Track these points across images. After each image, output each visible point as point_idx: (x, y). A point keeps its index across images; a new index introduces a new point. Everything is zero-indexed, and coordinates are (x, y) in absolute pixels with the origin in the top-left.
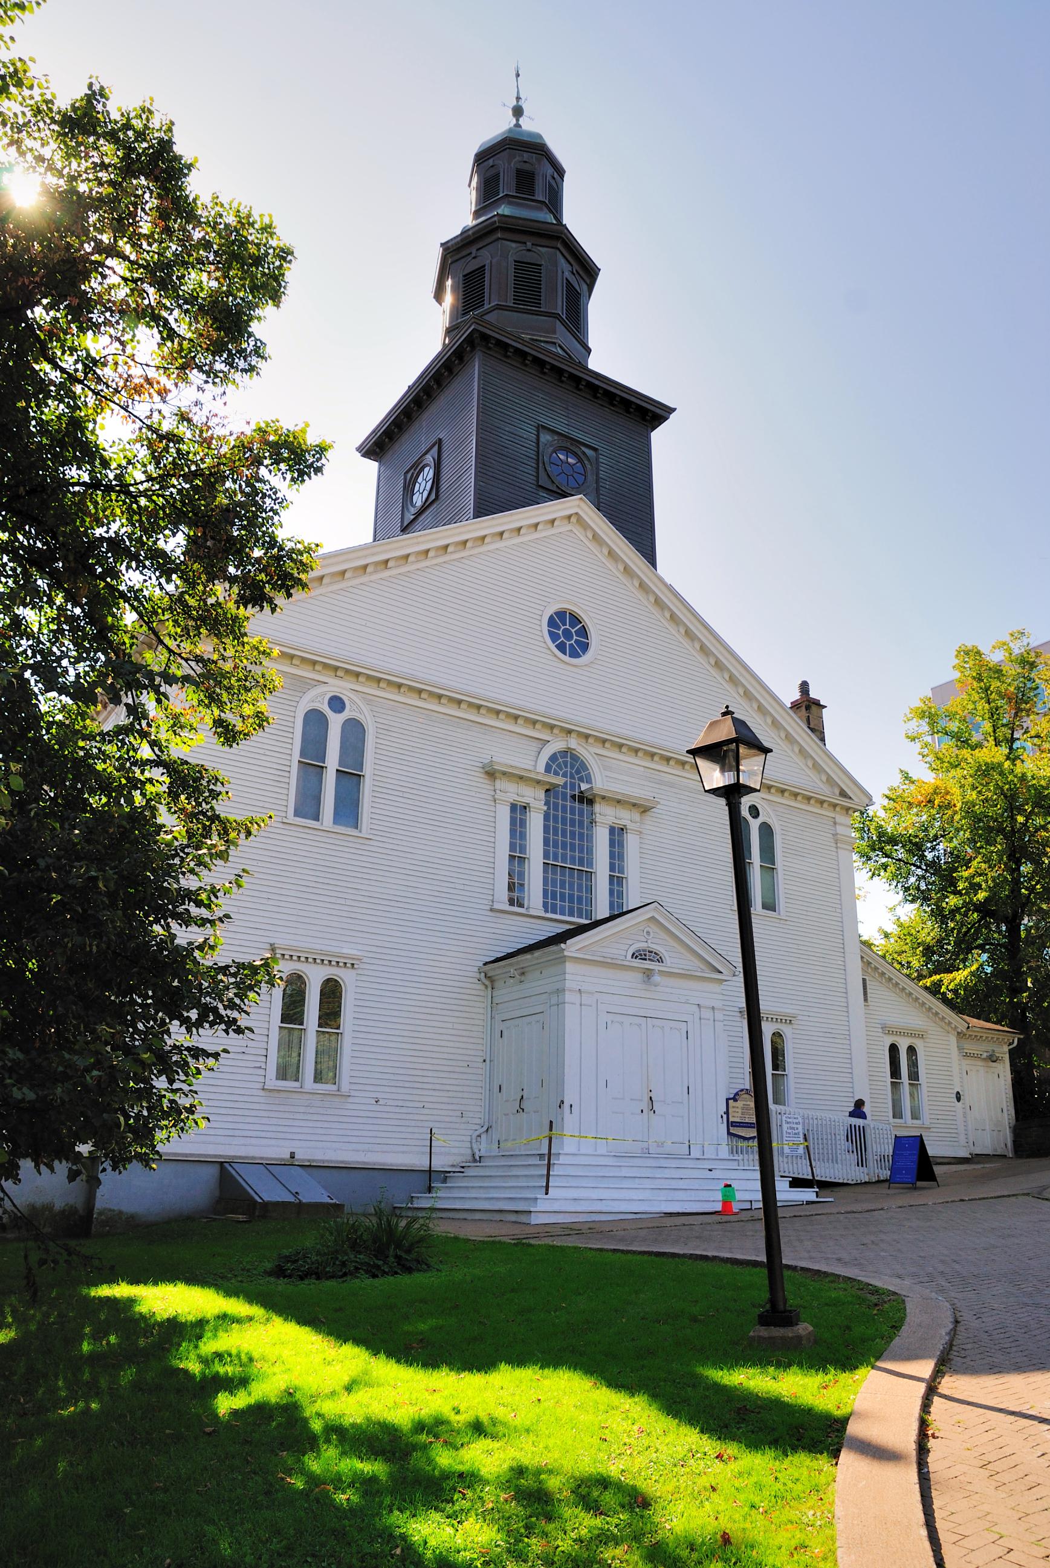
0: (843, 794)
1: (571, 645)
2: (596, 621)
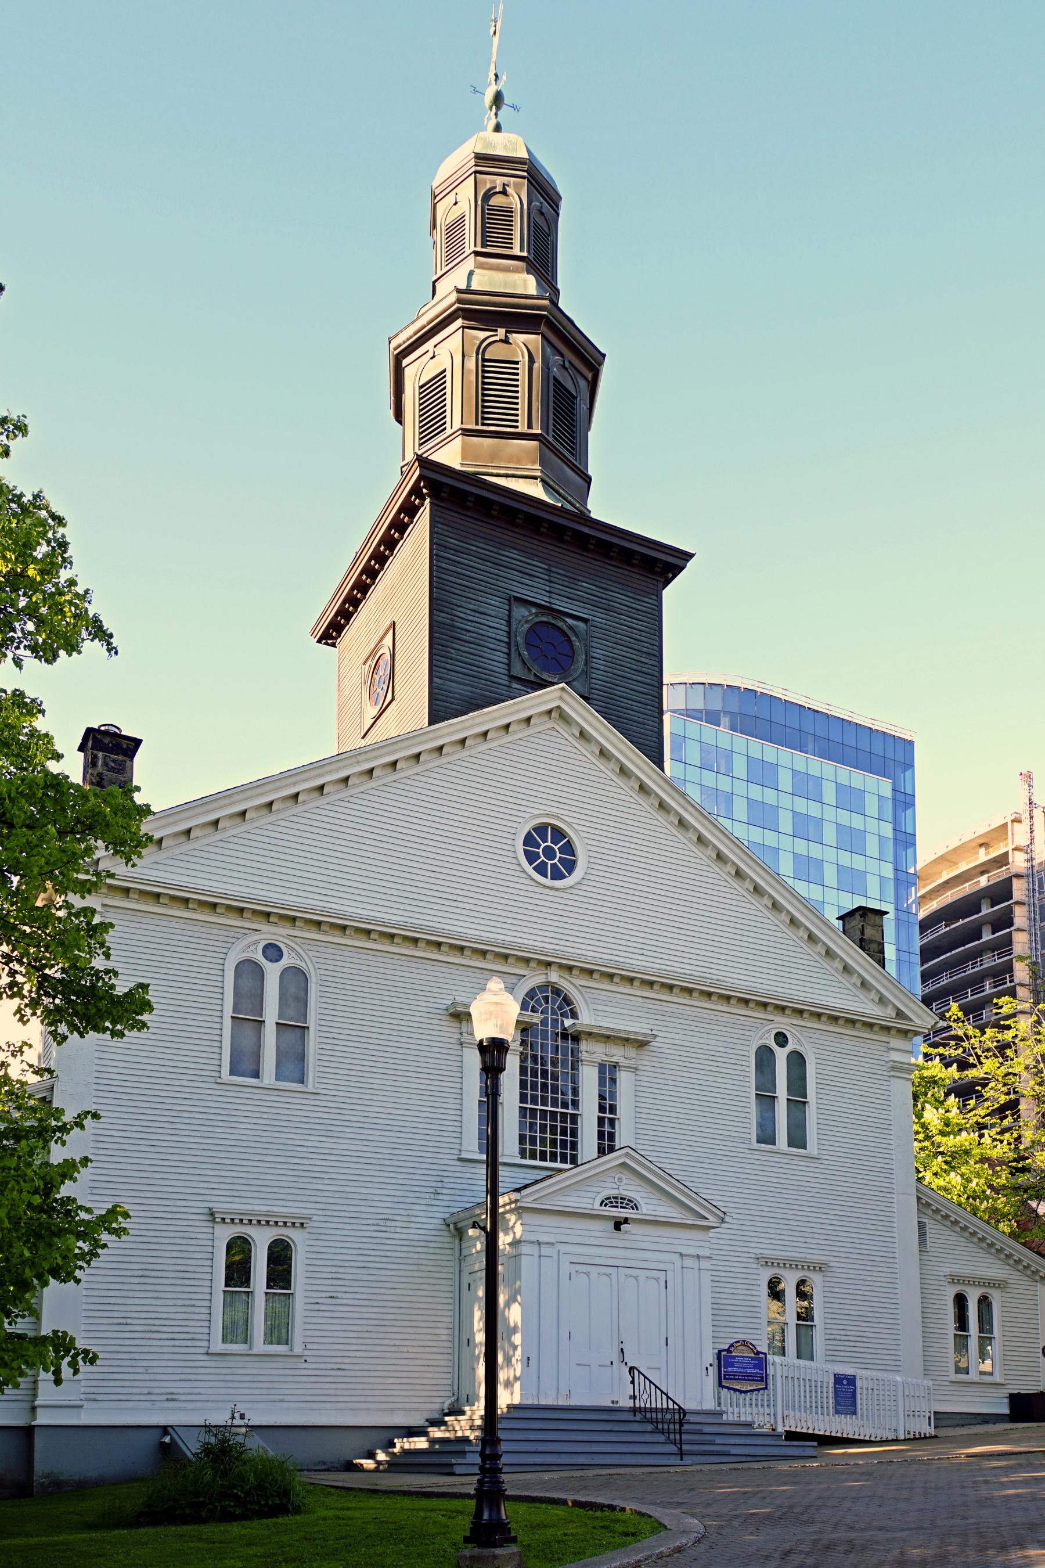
0: (900, 1014)
1: (553, 866)
2: (583, 834)
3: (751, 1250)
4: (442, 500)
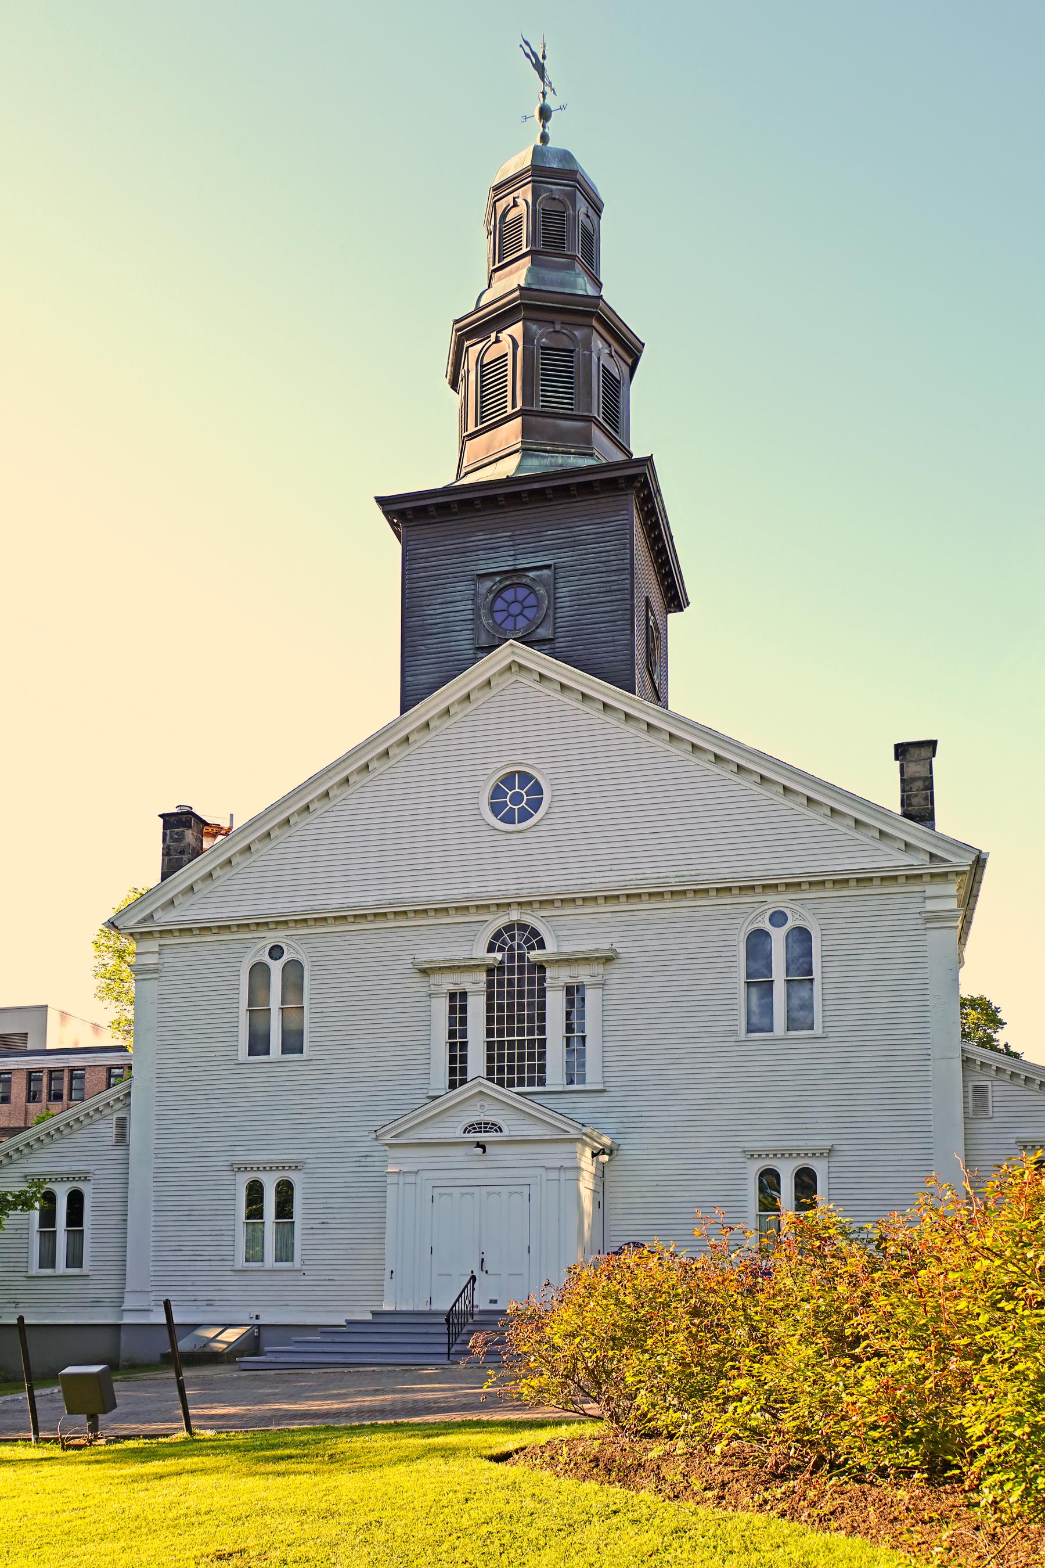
2: (546, 771)
3: (737, 1144)
4: (411, 521)
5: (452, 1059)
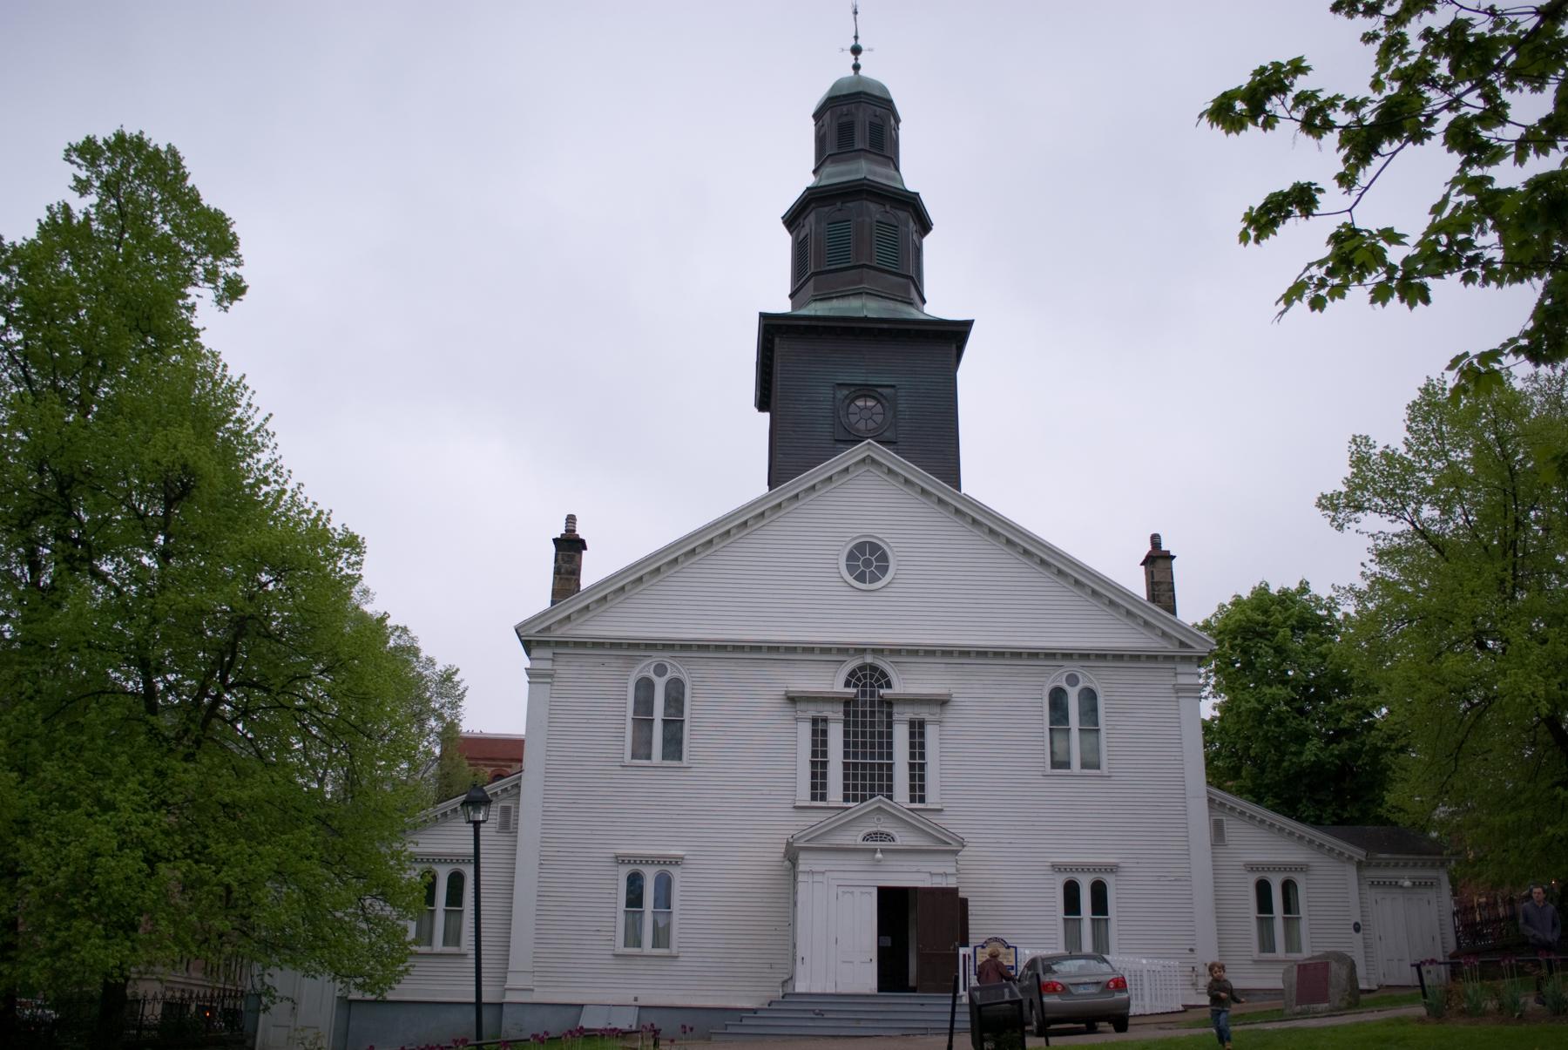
0: (1182, 644)
5: (814, 776)
